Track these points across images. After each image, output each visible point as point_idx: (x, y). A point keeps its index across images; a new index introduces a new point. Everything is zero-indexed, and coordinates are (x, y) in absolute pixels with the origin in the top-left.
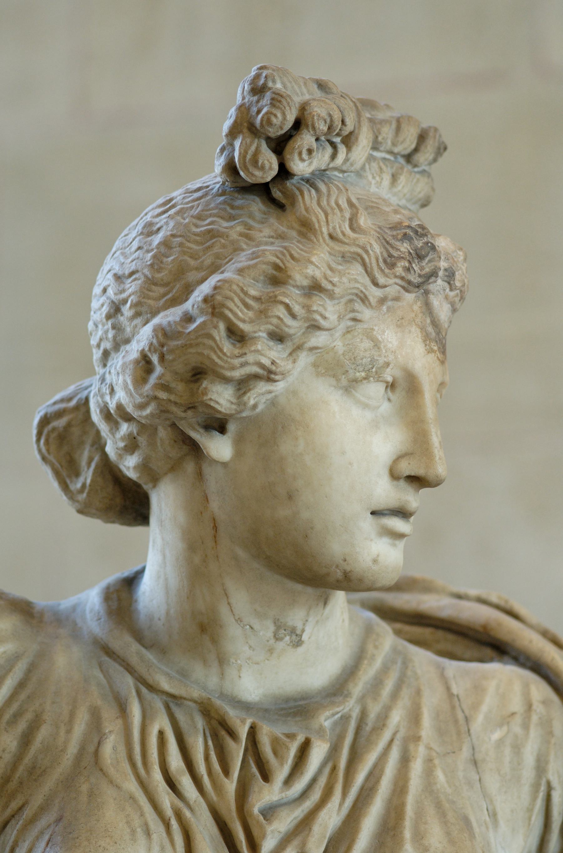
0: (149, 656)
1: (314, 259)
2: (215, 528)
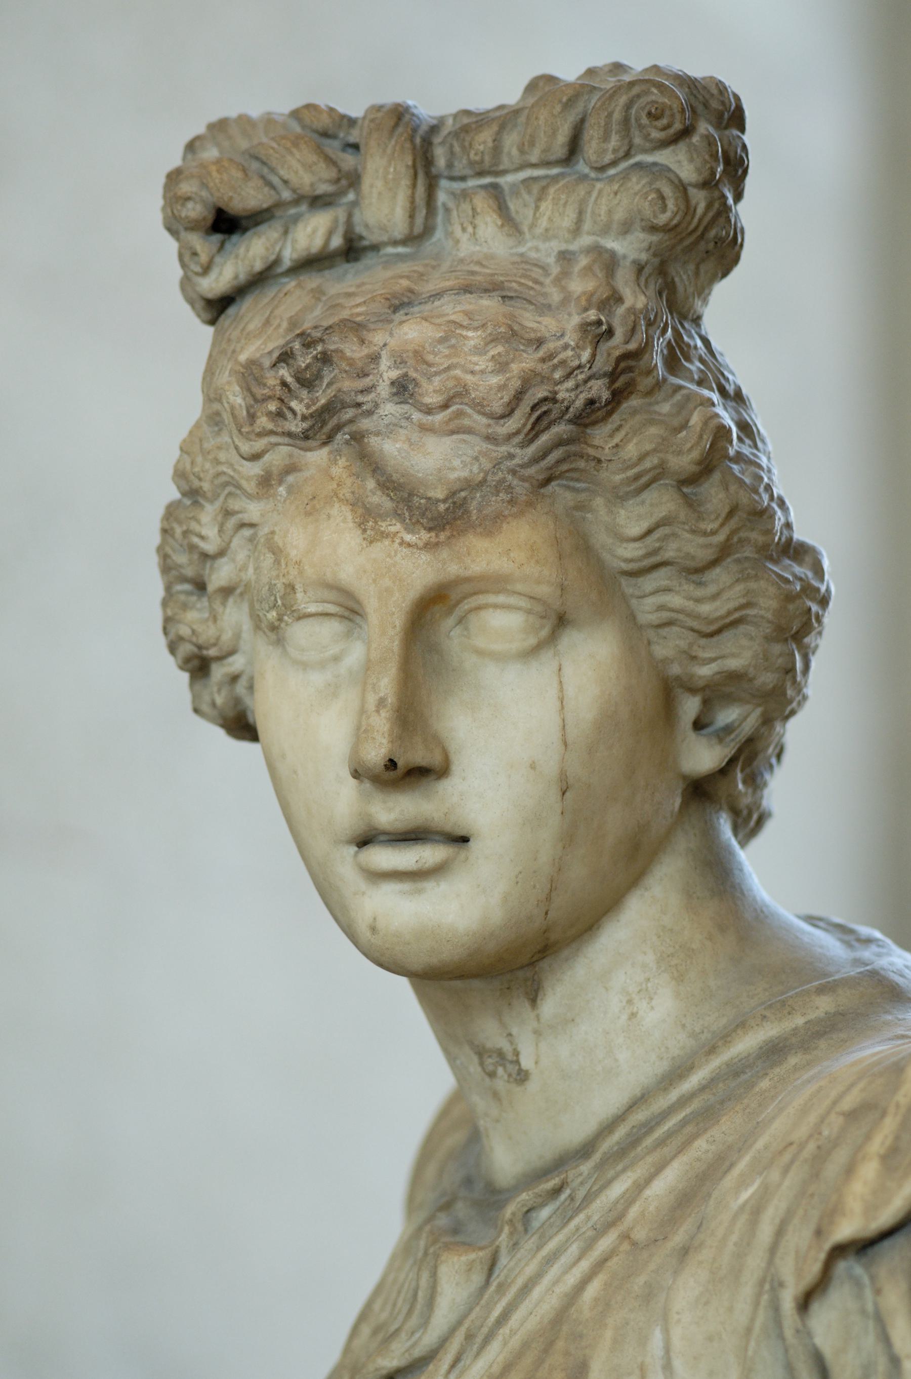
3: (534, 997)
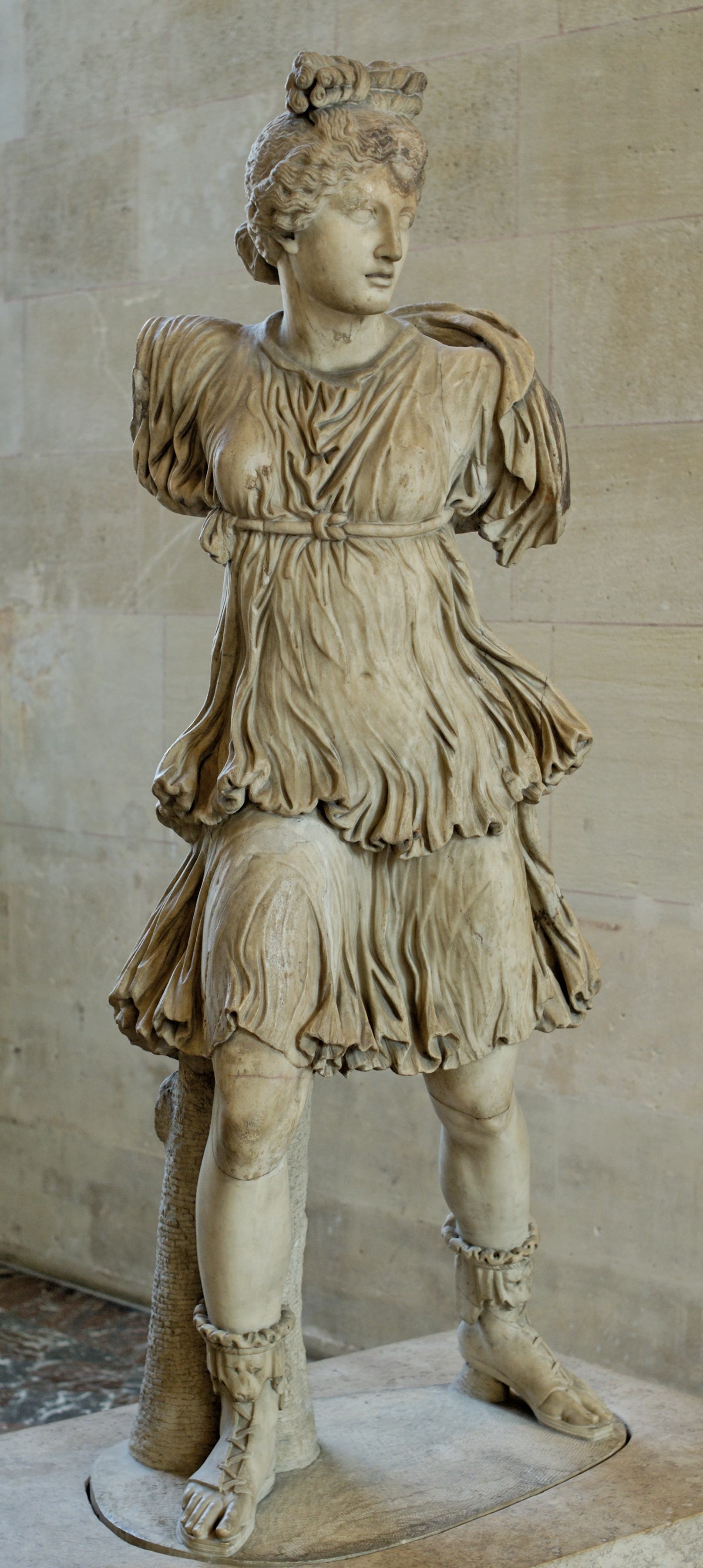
0: (280, 351)
1: (323, 150)
2: (298, 286)
3: (361, 321)
